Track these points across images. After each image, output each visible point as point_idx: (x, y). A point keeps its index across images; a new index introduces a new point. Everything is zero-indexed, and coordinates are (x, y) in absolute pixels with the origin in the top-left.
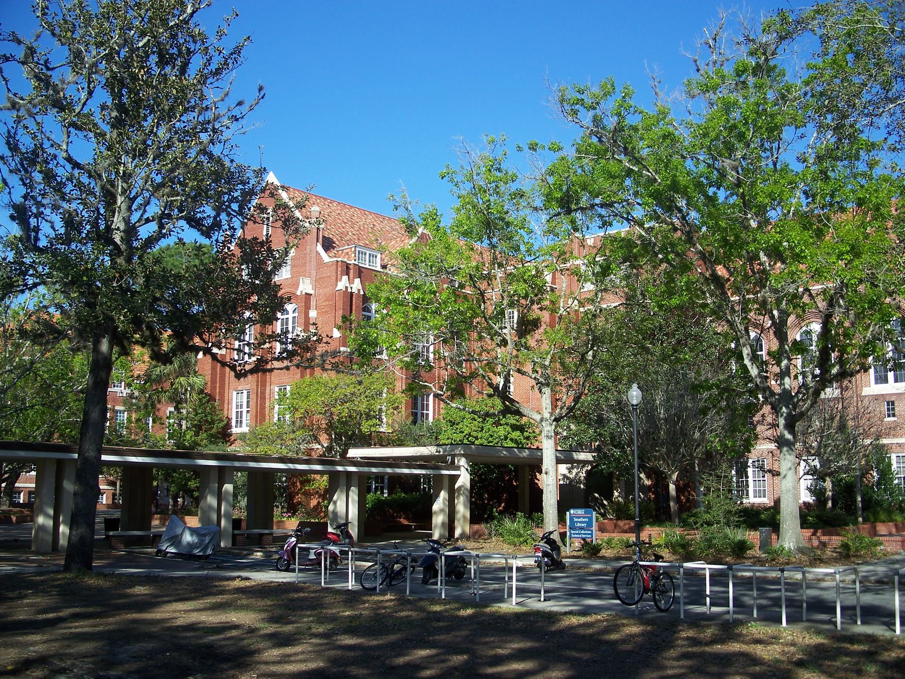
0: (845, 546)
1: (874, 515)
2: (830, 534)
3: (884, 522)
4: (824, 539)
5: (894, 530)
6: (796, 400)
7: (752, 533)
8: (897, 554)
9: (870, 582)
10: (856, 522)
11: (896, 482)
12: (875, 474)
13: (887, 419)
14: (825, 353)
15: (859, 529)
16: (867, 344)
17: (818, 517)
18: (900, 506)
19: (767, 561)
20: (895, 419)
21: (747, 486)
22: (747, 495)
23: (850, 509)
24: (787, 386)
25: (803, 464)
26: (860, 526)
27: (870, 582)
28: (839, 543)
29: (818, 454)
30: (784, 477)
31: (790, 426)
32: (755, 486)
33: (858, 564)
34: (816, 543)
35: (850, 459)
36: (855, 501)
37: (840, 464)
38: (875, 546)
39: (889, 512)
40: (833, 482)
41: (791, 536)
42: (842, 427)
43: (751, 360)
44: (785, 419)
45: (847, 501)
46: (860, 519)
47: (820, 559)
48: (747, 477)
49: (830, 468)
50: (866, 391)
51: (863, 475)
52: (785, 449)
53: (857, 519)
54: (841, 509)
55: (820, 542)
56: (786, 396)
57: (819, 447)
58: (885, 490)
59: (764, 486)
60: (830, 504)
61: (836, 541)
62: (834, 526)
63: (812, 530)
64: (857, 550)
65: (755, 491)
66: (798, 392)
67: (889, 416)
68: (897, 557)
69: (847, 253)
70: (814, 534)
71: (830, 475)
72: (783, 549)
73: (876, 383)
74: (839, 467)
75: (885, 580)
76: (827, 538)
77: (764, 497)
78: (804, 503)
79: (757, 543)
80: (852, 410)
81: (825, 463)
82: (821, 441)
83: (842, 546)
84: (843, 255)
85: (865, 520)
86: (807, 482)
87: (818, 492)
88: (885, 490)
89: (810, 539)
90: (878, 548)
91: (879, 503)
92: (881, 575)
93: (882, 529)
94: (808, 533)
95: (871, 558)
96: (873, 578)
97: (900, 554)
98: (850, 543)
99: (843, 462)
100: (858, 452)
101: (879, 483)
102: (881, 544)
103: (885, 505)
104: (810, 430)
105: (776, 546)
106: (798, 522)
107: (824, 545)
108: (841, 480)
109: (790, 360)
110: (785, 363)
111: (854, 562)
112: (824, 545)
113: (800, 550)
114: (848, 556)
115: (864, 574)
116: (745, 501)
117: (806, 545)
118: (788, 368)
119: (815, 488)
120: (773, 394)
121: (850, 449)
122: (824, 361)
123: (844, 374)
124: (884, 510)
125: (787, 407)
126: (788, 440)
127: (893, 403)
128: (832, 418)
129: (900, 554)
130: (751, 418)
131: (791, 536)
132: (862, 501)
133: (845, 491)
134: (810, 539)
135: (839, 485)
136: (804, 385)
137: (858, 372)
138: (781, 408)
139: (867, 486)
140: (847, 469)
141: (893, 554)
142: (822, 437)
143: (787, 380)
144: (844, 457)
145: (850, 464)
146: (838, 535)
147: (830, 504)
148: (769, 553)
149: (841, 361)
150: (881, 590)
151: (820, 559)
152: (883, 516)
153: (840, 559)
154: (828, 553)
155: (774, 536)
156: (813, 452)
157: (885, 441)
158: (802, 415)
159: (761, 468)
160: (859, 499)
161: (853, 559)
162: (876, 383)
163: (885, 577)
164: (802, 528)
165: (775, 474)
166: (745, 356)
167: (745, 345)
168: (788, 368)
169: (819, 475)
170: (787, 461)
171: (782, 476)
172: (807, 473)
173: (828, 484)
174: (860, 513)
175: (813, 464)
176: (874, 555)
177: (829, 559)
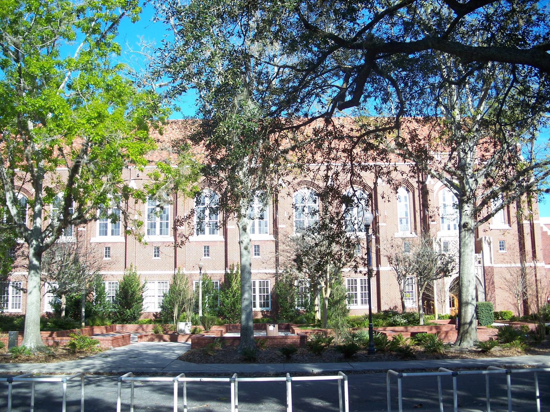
0: (73, 345)
1: (92, 321)
2: (62, 335)
3: (98, 325)
4: (58, 339)
5: (104, 331)
6: (44, 235)
7: (5, 335)
8: (109, 349)
9: (90, 373)
10: (80, 327)
11: (107, 299)
12: (94, 294)
13: (105, 258)
14: (68, 201)
15: (82, 330)
16: (101, 195)
17: (55, 323)
18: (109, 315)
19: (11, 358)
20: (109, 258)
21: (7, 301)
22: (7, 306)
23: (77, 316)
24: (38, 225)
25: (47, 285)
26: (83, 329)
27: (90, 373)
28: (68, 342)
29: (57, 279)
30: (30, 293)
31: (38, 255)
32: (13, 301)
33: (82, 358)
34: (51, 342)
35: (79, 283)
36: (81, 312)
37: (73, 286)
38: (94, 344)
39: (102, 319)
40: (67, 299)
41: (33, 338)
42: (76, 261)
43: (12, 202)
44: (35, 249)
45: (75, 312)
46: (83, 324)
47: (53, 356)
48: (8, 294)
49: (65, 288)
50: (93, 240)
51: (87, 295)
52: (32, 272)
53: (81, 324)
54: (71, 316)
55: (55, 342)
56: (37, 233)
57: (59, 274)
58: (100, 305)
59: (20, 301)
60: (63, 314)
61: (66, 341)
62: (65, 329)
63: (50, 332)
64: (81, 348)
65: (13, 304)
66: (46, 230)
67: (106, 256)
68: (109, 352)
69: (95, 119)
70: (51, 335)
71: (65, 293)
72: (25, 348)
73: (100, 235)
74: (71, 288)
75: (101, 371)
76: (60, 338)
77: (19, 308)
78: (47, 313)
79: (6, 343)
80: (83, 251)
81: (62, 285)
82: (61, 269)
83: (70, 345)
84: (91, 120)
85: (87, 325)
86: (49, 298)
87: (57, 306)
88: (100, 305)
89: (47, 340)
90: (96, 345)
91: (96, 313)
92: (98, 367)
93: (97, 330)
94: (46, 334)
95: (91, 353)
96: (92, 371)
97: (111, 349)
98: (76, 342)
99: (75, 285)
100: (85, 278)
101: (96, 300)
102: (98, 342)
103: (100, 314)
104: (54, 261)
105: (20, 346)
106: (39, 327)
107: (57, 344)
108: (73, 297)
109: (42, 205)
110: (38, 207)
111: (78, 357)
112: (57, 344)
113: (39, 349)
114: (74, 353)
115: (86, 367)
116: (5, 311)
117: (44, 344)
118: (40, 211)
119: (55, 303)
120: (26, 230)
121: (80, 277)
122: (66, 211)
123: (82, 220)
124: (99, 317)
125: (37, 240)
126: (35, 265)
127: (109, 248)
128: (70, 254)
129: (111, 349)
130: (14, 253)
131: (33, 338)
132: (85, 312)
133: (75, 305)
134: (47, 340)
135: (71, 301)
136: (51, 225)
137: (91, 220)
138: (32, 241)
139: (89, 301)
140: (78, 290)
141: (106, 350)
142: (61, 266)
143: (38, 220)
144: (75, 281)
145: (79, 286)
146: (69, 336)
147: (63, 314)
148: (13, 352)
149: (79, 209)
150: (99, 381)
151: (53, 356)
152: (98, 322)
153: (68, 355)
154: (60, 350)
155: (20, 337)
156: (54, 277)
157: (101, 272)
158: (47, 246)
159: (16, 287)
160: (83, 310)
161: (78, 355)
162: (100, 235)
163: (102, 369)
164: (41, 330)
165: (25, 291)
166: (8, 199)
167: (8, 191)
168: (40, 211)
169: (59, 293)
170: (34, 280)
171: (28, 292)
172: (49, 292)
173: (63, 300)
174: (83, 319)
175: (54, 285)
176: (92, 351)
177: (60, 355)
